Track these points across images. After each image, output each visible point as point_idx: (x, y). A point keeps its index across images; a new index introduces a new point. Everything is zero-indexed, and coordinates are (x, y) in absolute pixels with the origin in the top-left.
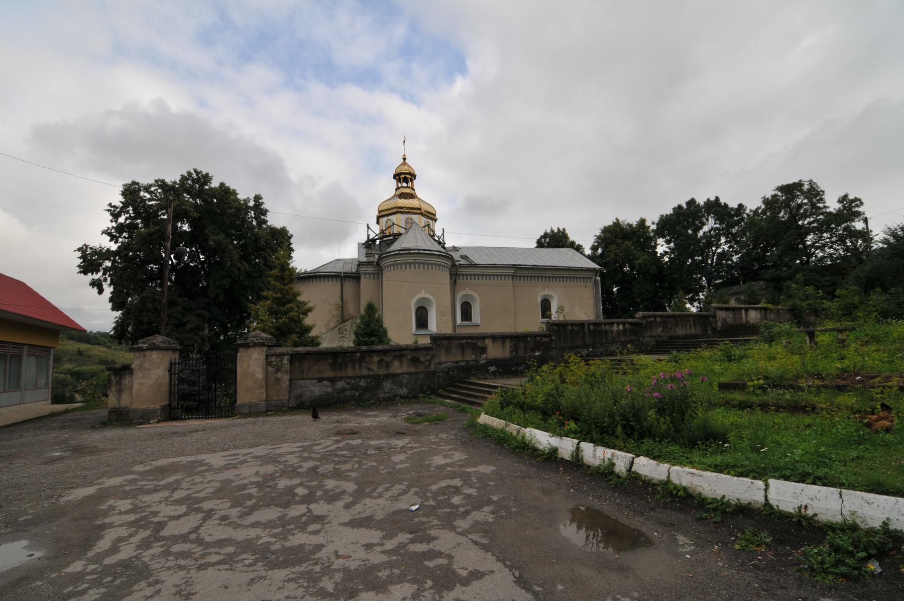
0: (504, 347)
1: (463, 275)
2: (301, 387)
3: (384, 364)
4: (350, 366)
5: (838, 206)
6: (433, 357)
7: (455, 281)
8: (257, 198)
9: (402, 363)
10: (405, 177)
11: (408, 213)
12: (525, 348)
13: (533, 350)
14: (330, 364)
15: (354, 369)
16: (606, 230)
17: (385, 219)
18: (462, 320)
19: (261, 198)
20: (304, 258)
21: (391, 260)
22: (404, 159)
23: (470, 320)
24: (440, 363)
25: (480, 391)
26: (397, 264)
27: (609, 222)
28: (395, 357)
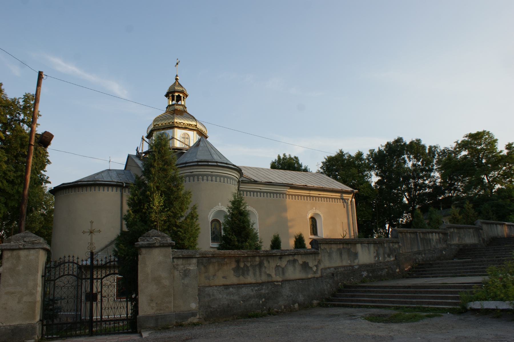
2: (209, 295)
3: (280, 269)
4: (251, 273)
5: (505, 152)
6: (319, 262)
10: (175, 94)
11: (185, 128)
13: (389, 256)
14: (233, 269)
15: (255, 274)
21: (187, 171)
22: (177, 79)
24: (326, 269)
25: (373, 291)
26: (194, 176)
27: (333, 153)
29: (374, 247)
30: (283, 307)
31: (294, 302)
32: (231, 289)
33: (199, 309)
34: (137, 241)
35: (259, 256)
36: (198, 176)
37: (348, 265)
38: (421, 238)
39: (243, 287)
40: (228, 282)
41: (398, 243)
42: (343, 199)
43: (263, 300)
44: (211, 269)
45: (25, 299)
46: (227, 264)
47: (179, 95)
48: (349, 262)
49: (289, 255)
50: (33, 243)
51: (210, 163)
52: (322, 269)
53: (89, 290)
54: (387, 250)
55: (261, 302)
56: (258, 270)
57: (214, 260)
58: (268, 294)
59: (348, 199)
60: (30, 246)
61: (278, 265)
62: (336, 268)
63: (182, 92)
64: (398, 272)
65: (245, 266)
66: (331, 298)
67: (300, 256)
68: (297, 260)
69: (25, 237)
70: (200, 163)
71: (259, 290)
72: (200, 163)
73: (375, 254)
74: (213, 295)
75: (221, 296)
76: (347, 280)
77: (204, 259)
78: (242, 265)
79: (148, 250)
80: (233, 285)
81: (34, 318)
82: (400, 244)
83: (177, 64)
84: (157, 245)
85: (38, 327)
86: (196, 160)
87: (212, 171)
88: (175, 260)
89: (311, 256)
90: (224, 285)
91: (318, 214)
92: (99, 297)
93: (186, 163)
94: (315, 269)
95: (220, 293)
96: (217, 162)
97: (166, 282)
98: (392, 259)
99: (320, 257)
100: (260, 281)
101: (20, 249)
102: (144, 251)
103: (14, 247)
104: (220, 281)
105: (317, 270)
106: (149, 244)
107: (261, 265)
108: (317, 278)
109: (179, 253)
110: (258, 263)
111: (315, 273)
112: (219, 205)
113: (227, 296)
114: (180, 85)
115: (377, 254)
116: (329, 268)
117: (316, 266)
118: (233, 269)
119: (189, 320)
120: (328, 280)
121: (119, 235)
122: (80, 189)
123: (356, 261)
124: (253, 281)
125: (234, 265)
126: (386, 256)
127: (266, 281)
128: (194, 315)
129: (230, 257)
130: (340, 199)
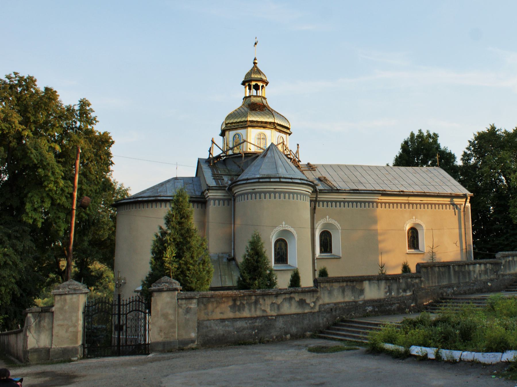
0: (379, 288)
1: (323, 201)
2: (207, 327)
3: (276, 306)
6: (318, 299)
7: (315, 208)
8: (84, 104)
9: (291, 305)
10: (253, 80)
12: (398, 289)
13: (405, 291)
14: (230, 307)
15: (250, 310)
16: (481, 137)
17: (232, 133)
18: (321, 252)
19: (89, 105)
20: (131, 173)
21: (248, 188)
22: (255, 63)
23: (330, 251)
24: (324, 305)
26: (256, 193)
27: (484, 128)
28: (285, 299)
29: (386, 283)
30: (275, 337)
31: (286, 334)
32: (227, 322)
33: (198, 337)
34: (151, 287)
35: (255, 295)
36: (260, 193)
37: (351, 300)
38: (455, 271)
40: (225, 316)
41: (421, 277)
42: (453, 204)
43: (256, 331)
44: (210, 307)
45: (71, 329)
46: (224, 302)
47: (256, 84)
48: (353, 298)
49: (285, 293)
50: (75, 290)
51: (272, 180)
52: (320, 305)
53: (117, 323)
54: (403, 286)
55: (254, 333)
56: (253, 307)
57: (213, 300)
58: (261, 326)
59: (461, 205)
60: (73, 292)
61: (274, 302)
62: (335, 304)
64: (413, 307)
65: (241, 303)
66: (325, 330)
67: (297, 294)
68: (294, 298)
69: (69, 285)
70: (261, 180)
71: (252, 323)
72: (261, 180)
73: (387, 290)
74: (210, 327)
75: (217, 328)
76: (348, 315)
77: (204, 299)
78: (238, 303)
79: (158, 293)
80: (229, 319)
81: (77, 342)
82: (422, 279)
83: (256, 44)
84: (165, 289)
85: (80, 349)
86: (258, 176)
88: (180, 301)
89: (309, 293)
90: (221, 319)
91: (419, 225)
92: (124, 327)
93: (247, 179)
94: (312, 305)
95: (216, 325)
96: (280, 178)
97: (172, 318)
98: (409, 293)
99: (319, 294)
100: (255, 316)
101: (66, 294)
102: (155, 294)
103: (62, 293)
104: (218, 315)
105: (315, 306)
106: (159, 289)
107: (256, 302)
108: (314, 313)
109: (184, 294)
110: (254, 301)
111: (312, 308)
112: (282, 225)
113: (223, 327)
114: (259, 72)
115: (389, 290)
116: (328, 304)
117: (314, 302)
118: (230, 307)
119: (189, 346)
120: (325, 314)
121: (148, 276)
122: (141, 206)
123: (362, 298)
125: (231, 303)
126: (401, 291)
127: (261, 315)
128: (193, 341)
129: (227, 297)
130: (449, 204)
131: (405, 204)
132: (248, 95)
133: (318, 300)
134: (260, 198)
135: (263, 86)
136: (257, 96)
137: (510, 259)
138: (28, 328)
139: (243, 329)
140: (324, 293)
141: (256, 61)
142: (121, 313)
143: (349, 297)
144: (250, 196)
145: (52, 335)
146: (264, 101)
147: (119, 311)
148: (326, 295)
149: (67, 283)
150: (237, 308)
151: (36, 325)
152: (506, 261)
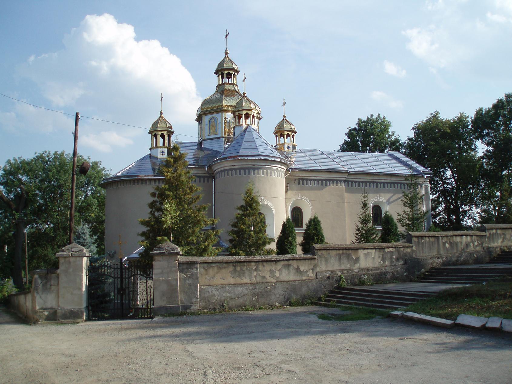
6: (315, 266)
14: (231, 272)
17: (208, 118)
22: (226, 54)
24: (321, 272)
39: (238, 287)
41: (412, 247)
44: (211, 271)
48: (349, 266)
53: (119, 286)
55: (254, 299)
57: (214, 265)
63: (233, 69)
69: (72, 248)
83: (227, 36)
87: (254, 164)
116: (326, 271)
123: (357, 265)
124: (249, 282)
131: (370, 182)
132: (221, 83)
133: (316, 268)
134: (240, 174)
135: (234, 75)
136: (229, 84)
137: (494, 231)
138: (36, 289)
139: (244, 295)
140: (321, 261)
141: (228, 52)
142: (124, 277)
143: (346, 265)
144: (230, 172)
145: (58, 297)
146: (236, 88)
147: (121, 275)
148: (323, 262)
149: (71, 246)
150: (237, 274)
151: (43, 285)
152: (490, 234)
